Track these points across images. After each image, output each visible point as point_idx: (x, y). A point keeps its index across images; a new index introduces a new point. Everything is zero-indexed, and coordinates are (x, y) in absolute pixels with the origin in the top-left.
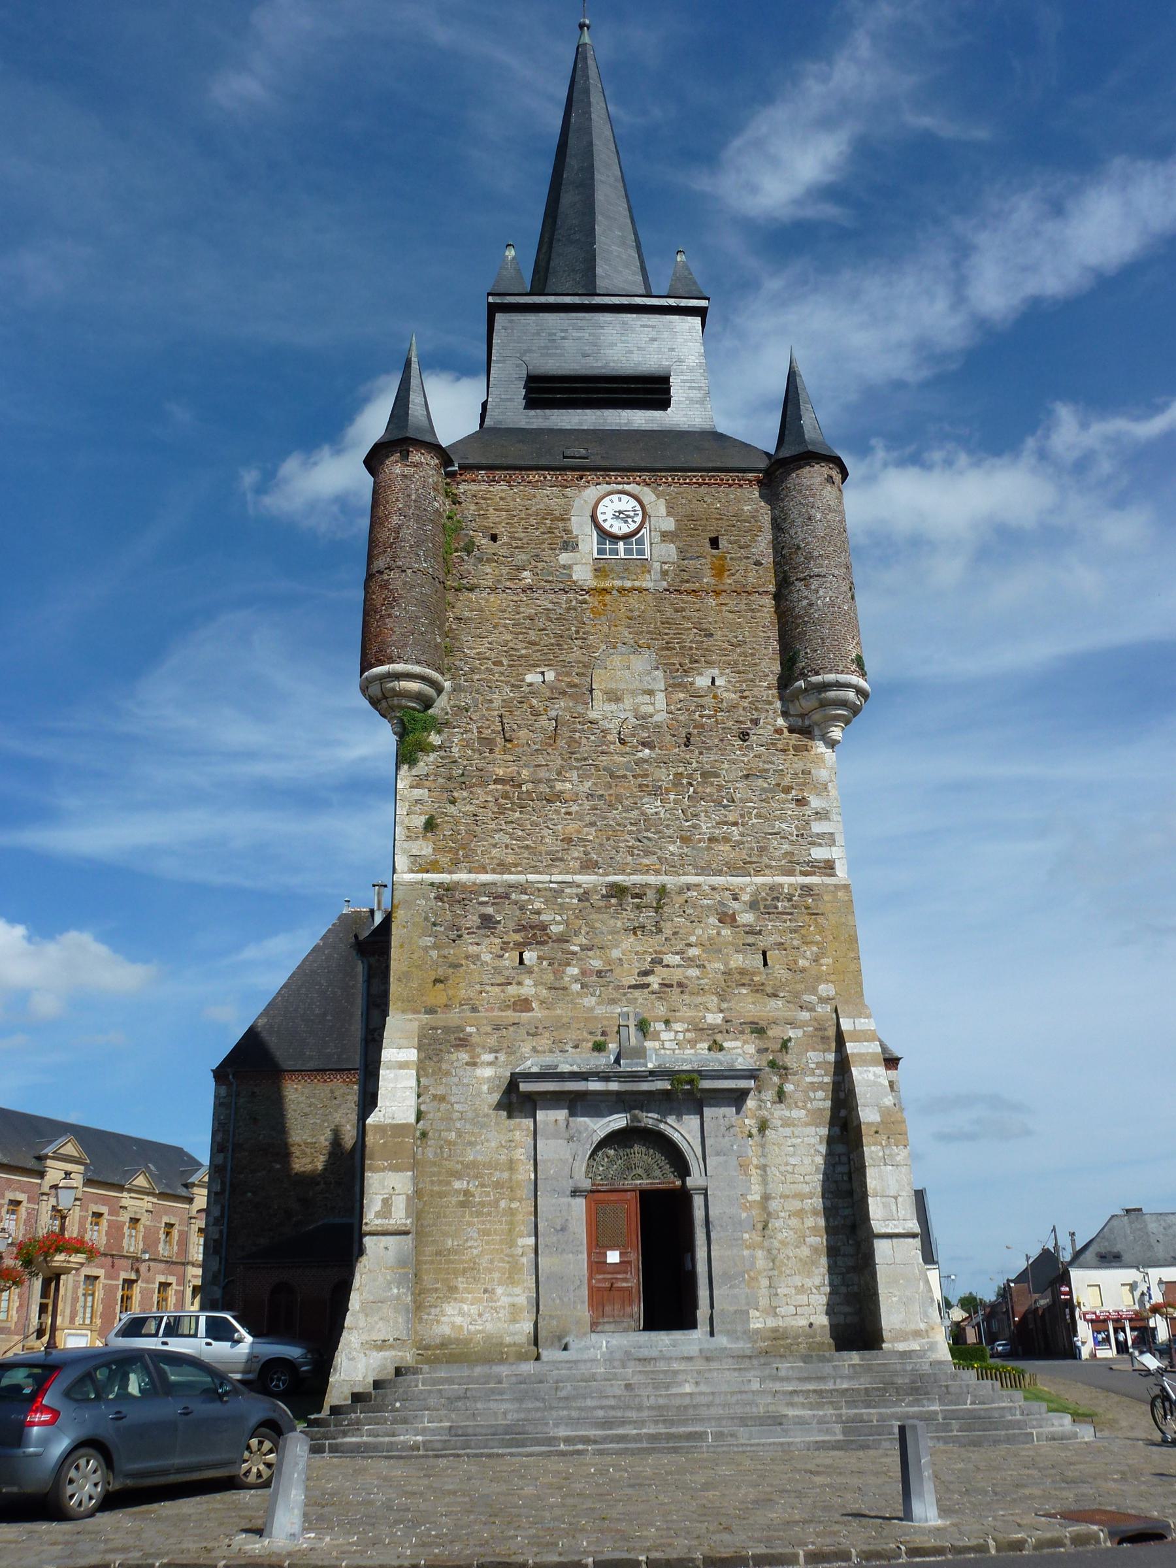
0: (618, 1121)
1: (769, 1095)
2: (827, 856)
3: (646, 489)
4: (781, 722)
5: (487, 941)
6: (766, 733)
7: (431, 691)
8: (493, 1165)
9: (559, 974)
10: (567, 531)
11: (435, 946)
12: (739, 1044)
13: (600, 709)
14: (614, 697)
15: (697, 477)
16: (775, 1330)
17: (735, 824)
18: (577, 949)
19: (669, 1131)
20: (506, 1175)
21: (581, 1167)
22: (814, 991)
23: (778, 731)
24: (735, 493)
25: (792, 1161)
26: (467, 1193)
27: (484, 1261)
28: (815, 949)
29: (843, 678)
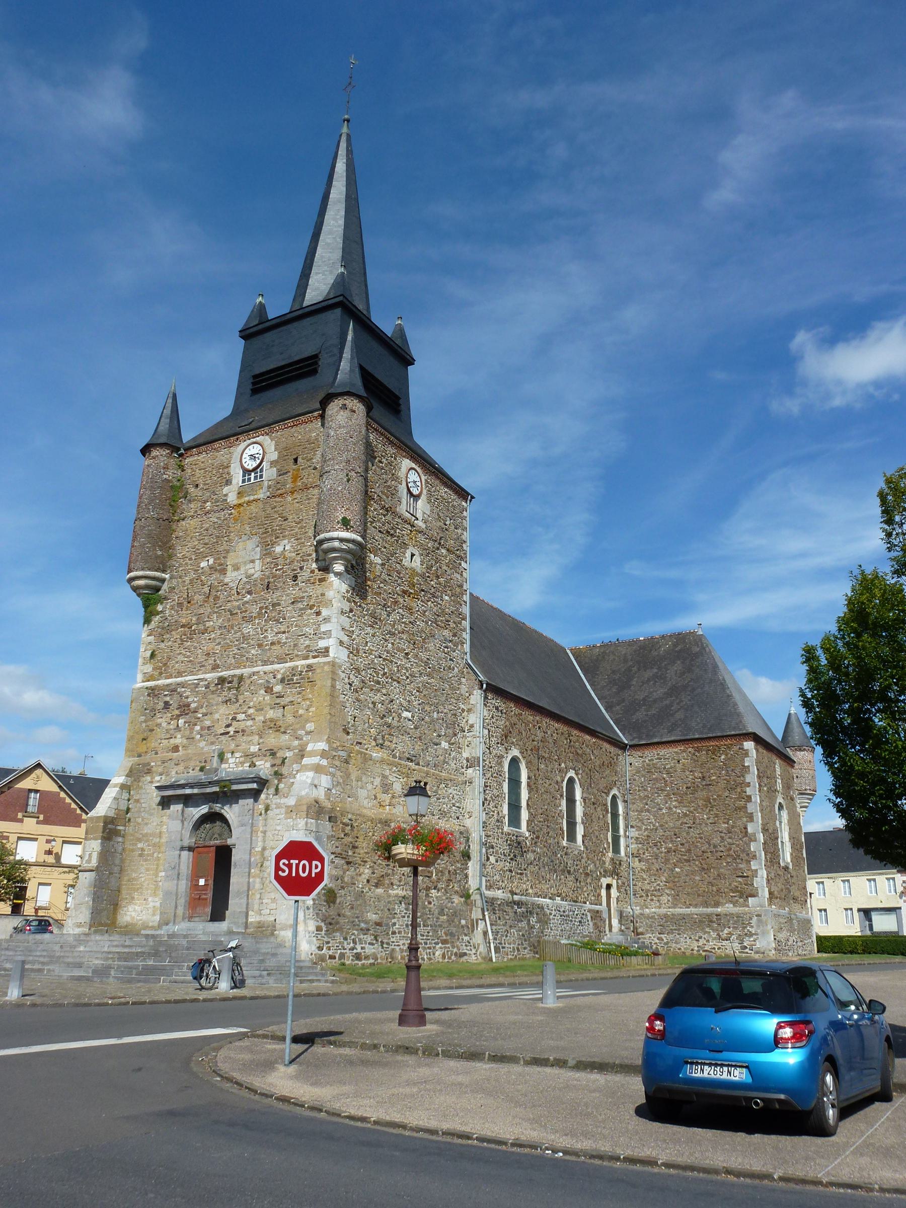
0: (204, 809)
1: (272, 790)
2: (327, 645)
3: (267, 437)
4: (314, 566)
5: (165, 716)
6: (306, 574)
7: (158, 583)
8: (153, 835)
9: (192, 730)
10: (229, 473)
11: (145, 721)
12: (262, 762)
13: (232, 577)
14: (236, 568)
15: (290, 422)
16: (259, 922)
17: (284, 632)
18: (200, 715)
19: (225, 814)
20: (158, 840)
21: (187, 834)
22: (303, 728)
23: (312, 572)
24: (309, 426)
25: (278, 828)
26: (143, 850)
27: (145, 884)
28: (308, 703)
29: (335, 534)
